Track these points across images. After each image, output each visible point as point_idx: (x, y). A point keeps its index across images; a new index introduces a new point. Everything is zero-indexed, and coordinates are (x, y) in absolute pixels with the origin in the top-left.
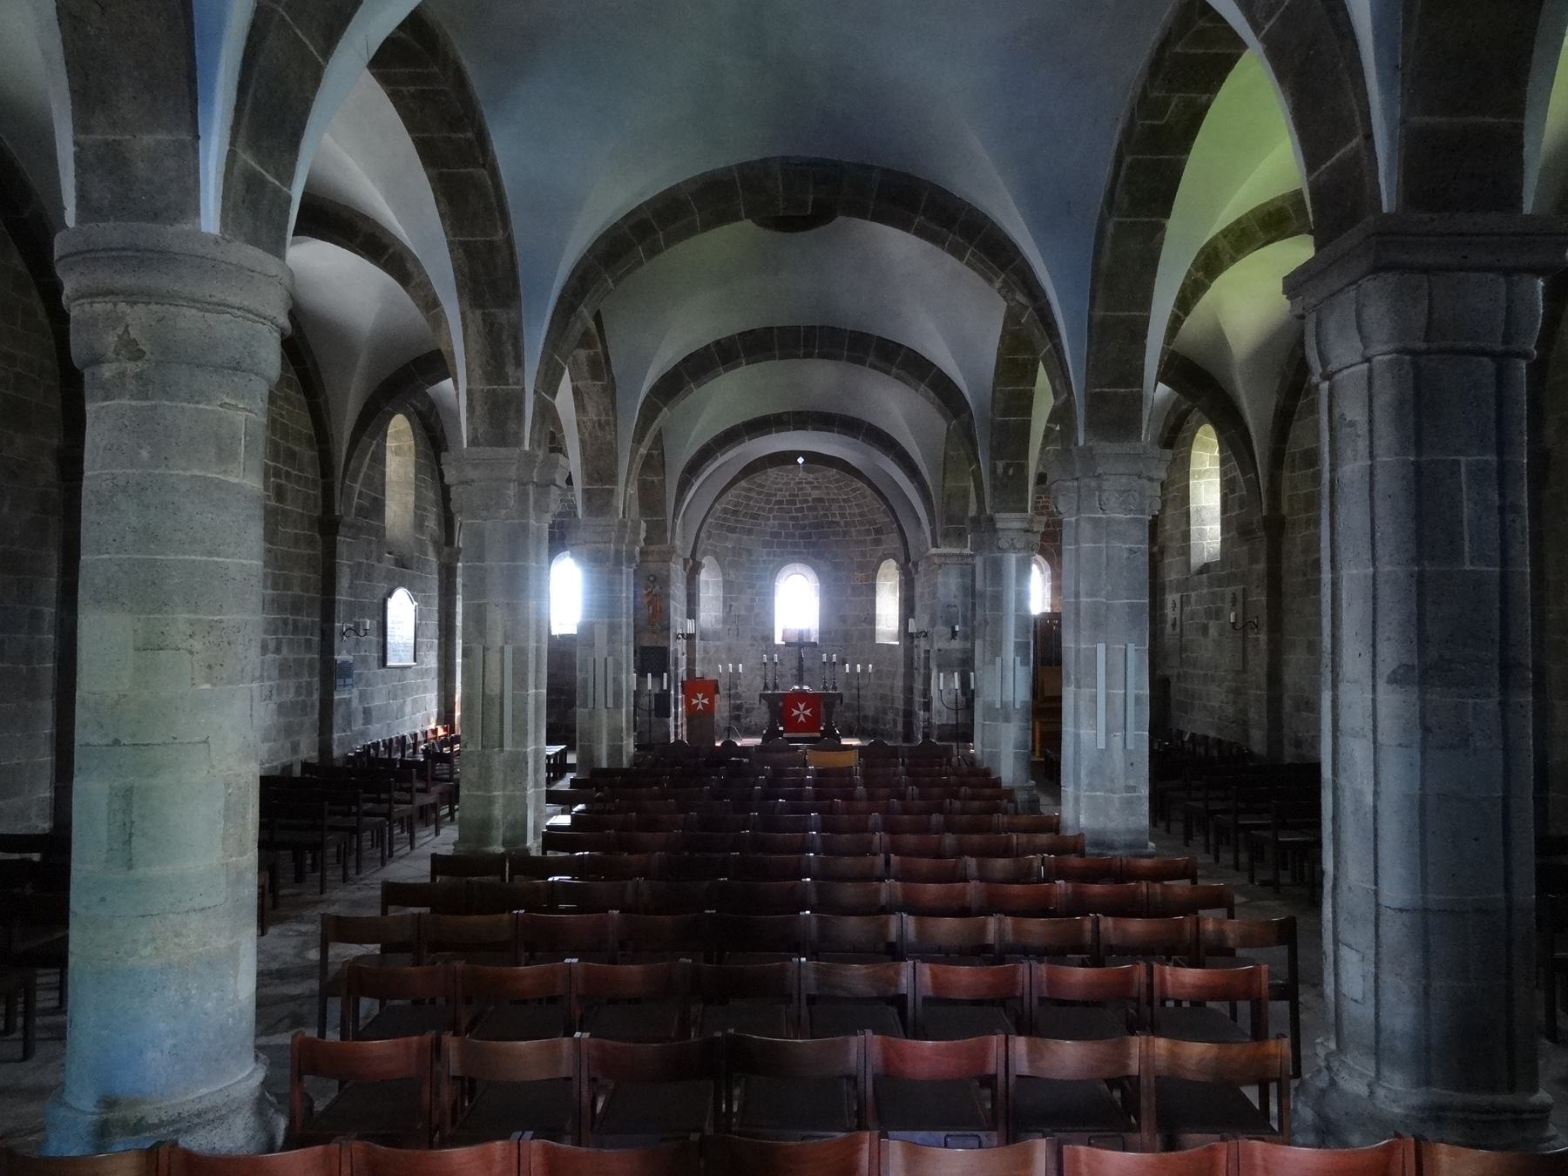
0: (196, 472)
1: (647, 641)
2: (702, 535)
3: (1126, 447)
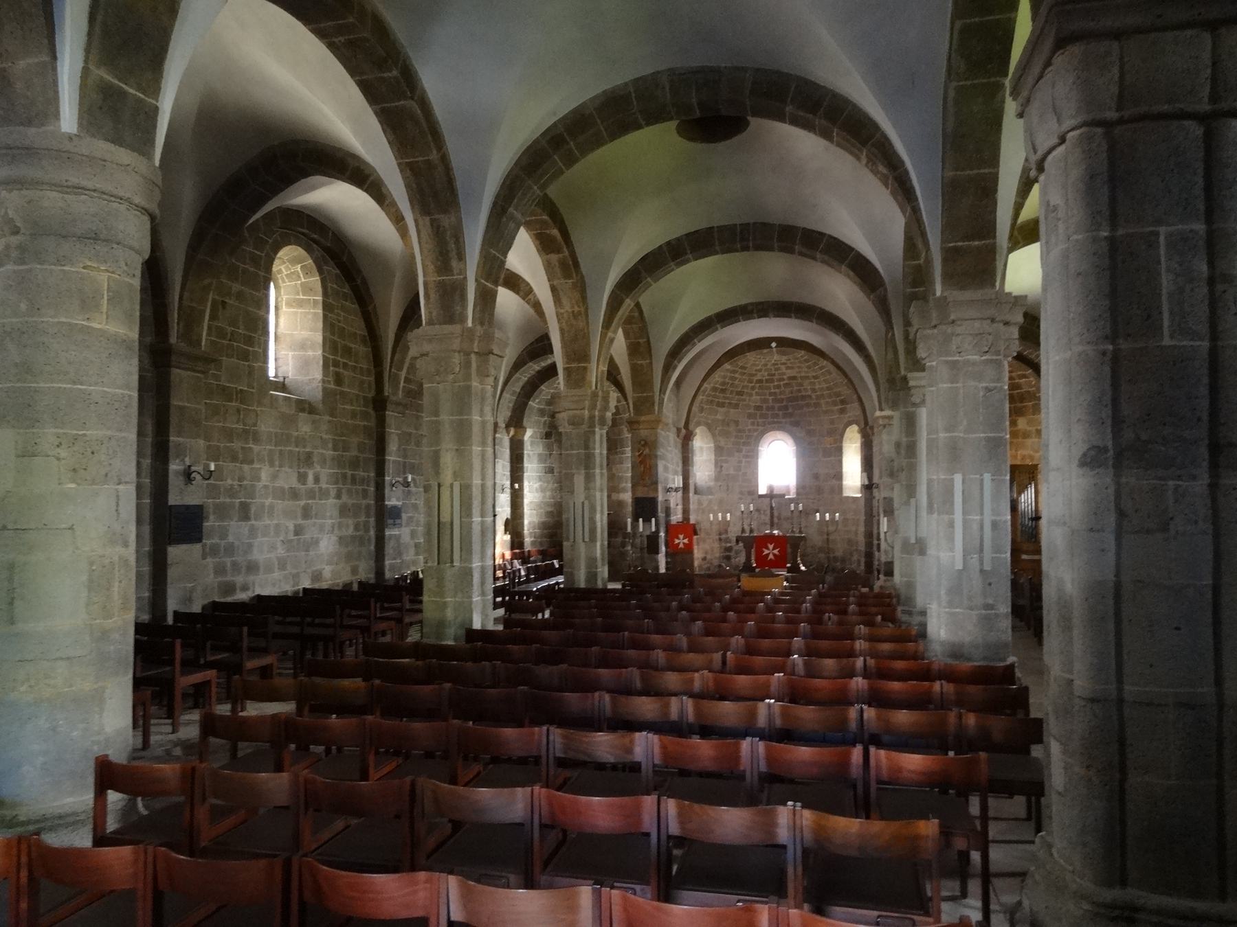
0: (63, 320)
1: (641, 493)
2: (694, 409)
3: (977, 294)
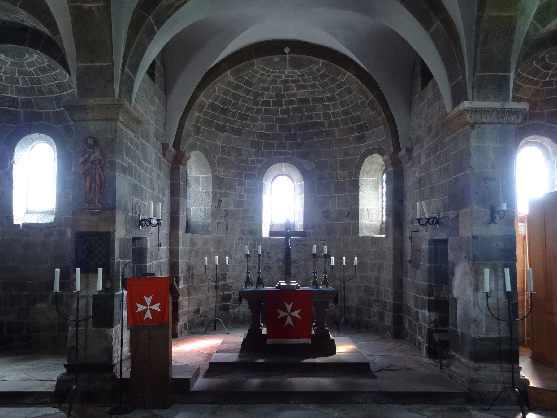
2: (188, 126)
